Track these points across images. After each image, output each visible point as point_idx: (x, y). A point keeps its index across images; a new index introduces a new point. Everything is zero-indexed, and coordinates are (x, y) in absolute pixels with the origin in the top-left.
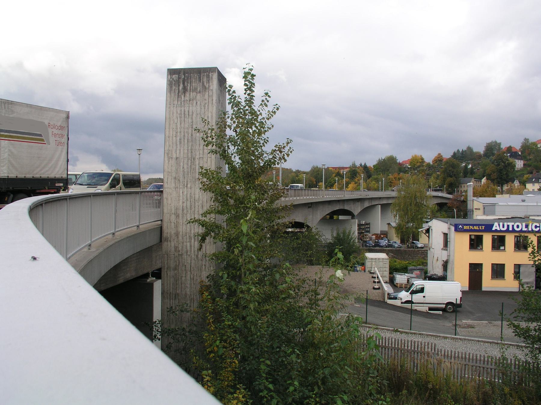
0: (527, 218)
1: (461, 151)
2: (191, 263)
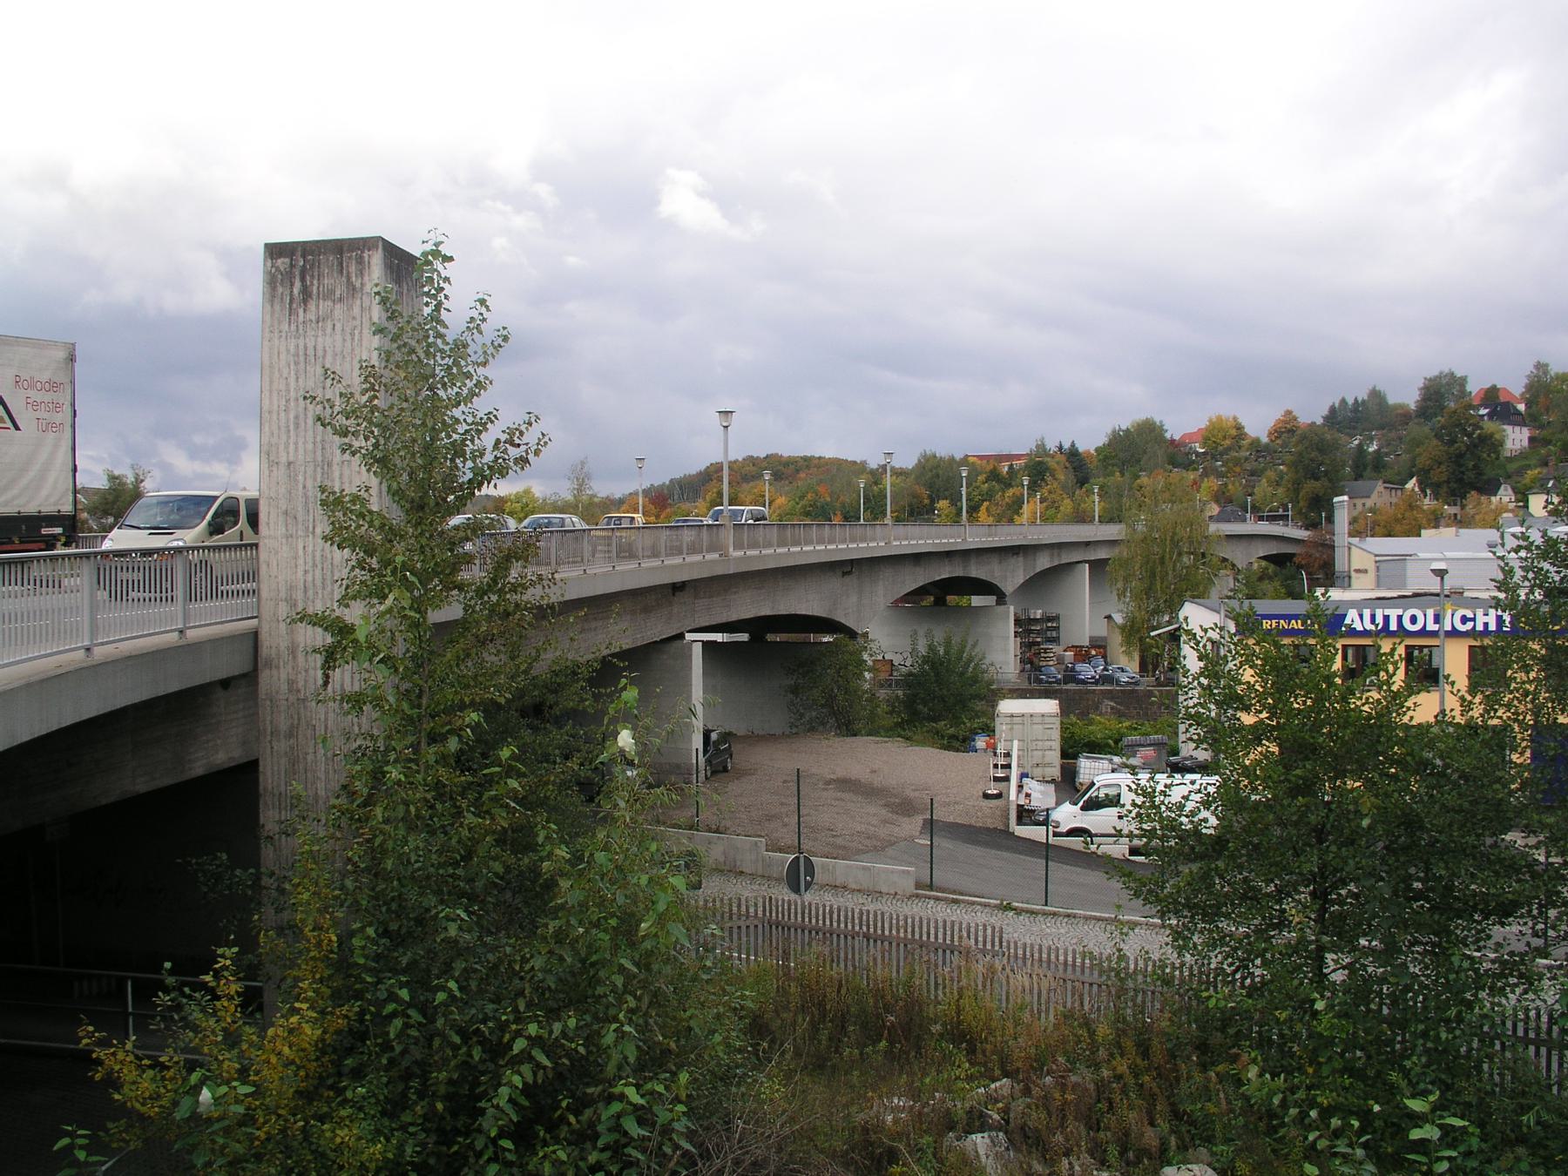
0: (1456, 596)
1: (1350, 401)
2: (326, 719)
